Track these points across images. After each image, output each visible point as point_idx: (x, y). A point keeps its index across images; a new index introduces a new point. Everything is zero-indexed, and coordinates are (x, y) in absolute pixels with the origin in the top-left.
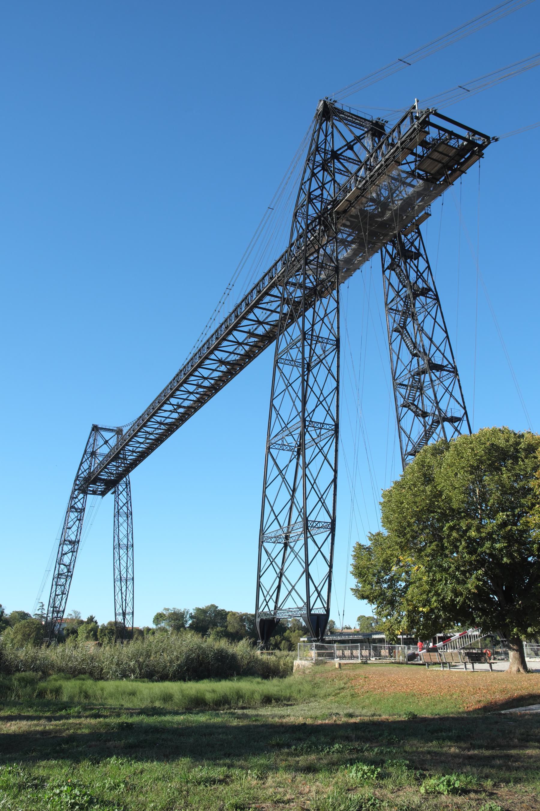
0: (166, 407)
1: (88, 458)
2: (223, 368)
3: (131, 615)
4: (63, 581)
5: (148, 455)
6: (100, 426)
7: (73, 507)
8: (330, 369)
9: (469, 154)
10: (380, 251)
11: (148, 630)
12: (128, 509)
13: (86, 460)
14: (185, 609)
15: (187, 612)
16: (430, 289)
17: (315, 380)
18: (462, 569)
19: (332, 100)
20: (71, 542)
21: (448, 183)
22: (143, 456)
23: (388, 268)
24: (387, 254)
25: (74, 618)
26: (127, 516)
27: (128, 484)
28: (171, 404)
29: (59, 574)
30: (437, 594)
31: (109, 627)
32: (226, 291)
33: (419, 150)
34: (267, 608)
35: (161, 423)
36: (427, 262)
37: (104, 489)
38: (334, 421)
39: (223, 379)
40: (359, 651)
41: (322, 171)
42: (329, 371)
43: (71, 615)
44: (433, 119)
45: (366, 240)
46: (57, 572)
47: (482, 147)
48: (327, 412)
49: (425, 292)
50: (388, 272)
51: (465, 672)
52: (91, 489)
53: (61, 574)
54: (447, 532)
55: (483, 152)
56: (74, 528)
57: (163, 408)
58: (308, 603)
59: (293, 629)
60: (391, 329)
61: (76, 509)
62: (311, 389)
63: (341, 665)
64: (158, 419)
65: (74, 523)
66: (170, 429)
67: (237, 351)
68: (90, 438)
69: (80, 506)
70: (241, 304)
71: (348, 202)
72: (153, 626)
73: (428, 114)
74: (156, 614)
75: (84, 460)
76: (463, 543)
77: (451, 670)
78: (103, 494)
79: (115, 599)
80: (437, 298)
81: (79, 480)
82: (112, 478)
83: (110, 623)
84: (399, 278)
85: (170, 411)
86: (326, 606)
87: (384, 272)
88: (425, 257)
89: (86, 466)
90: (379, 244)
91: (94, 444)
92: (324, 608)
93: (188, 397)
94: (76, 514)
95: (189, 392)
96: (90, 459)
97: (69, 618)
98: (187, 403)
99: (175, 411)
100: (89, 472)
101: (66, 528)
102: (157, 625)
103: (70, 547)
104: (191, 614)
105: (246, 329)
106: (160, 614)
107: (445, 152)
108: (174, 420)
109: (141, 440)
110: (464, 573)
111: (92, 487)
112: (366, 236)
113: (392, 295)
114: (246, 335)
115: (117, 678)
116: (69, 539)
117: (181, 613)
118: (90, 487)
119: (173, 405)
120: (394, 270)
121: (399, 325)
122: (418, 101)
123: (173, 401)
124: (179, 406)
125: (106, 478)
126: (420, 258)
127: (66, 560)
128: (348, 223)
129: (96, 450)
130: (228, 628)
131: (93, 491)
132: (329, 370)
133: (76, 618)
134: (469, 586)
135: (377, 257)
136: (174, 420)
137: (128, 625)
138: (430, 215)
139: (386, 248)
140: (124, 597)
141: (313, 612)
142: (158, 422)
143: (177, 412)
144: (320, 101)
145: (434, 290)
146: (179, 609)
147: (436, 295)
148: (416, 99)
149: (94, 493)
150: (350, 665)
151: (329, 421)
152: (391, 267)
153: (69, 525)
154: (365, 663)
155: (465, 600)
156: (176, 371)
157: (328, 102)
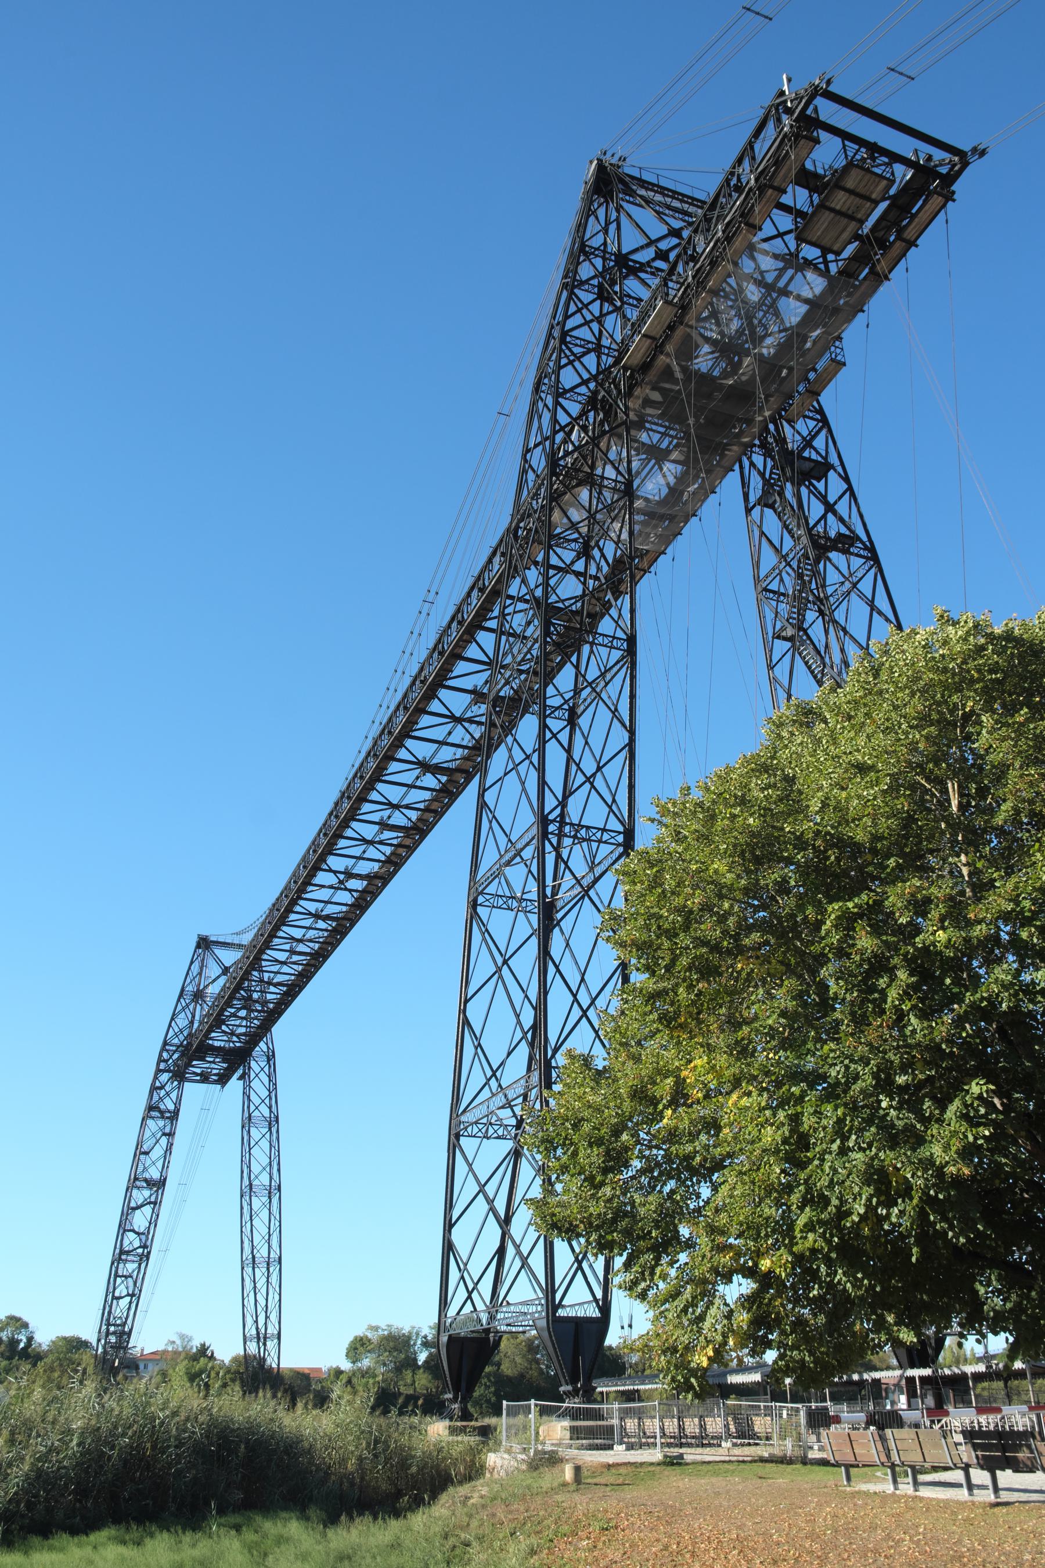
0: (321, 878)
1: (187, 1005)
2: (430, 781)
3: (276, 1341)
4: (131, 1267)
5: (301, 989)
6: (212, 939)
7: (156, 1108)
8: (616, 710)
9: (920, 202)
10: (737, 467)
11: (338, 1372)
12: (271, 1112)
13: (183, 1009)
14: (413, 1328)
15: (417, 1334)
16: (853, 539)
17: (587, 743)
18: (901, 1080)
19: (616, 157)
20: (150, 1183)
21: (879, 278)
22: (292, 991)
23: (759, 502)
24: (754, 473)
25: (180, 1349)
26: (270, 1124)
27: (270, 1057)
28: (330, 870)
29: (122, 1252)
30: (815, 1200)
31: (234, 1367)
32: (422, 607)
33: (799, 197)
34: (468, 1308)
35: (317, 916)
36: (846, 479)
37: (225, 1069)
38: (624, 825)
39: (433, 807)
40: (657, 1421)
41: (598, 302)
42: (613, 713)
43: (174, 1342)
44: (827, 109)
45: (689, 403)
46: (117, 1251)
47: (950, 179)
48: (610, 807)
49: (845, 543)
50: (756, 512)
51: (962, 1504)
52: (198, 1071)
53: (128, 1253)
54: (835, 938)
55: (953, 188)
56: (158, 1152)
57: (317, 880)
58: (550, 1289)
59: (640, 1367)
60: (770, 635)
61: (162, 1112)
62: (578, 765)
63: (585, 1473)
64: (312, 907)
65: (157, 1141)
66: (340, 929)
67: (453, 739)
68: (192, 963)
69: (171, 1107)
70: (449, 626)
71: (649, 341)
72: (346, 1365)
73: (815, 92)
74: (351, 1338)
75: (179, 1008)
76: (902, 975)
77: (925, 1492)
78: (223, 1079)
79: (243, 1305)
80: (873, 557)
81: (167, 1051)
82: (238, 1045)
83: (235, 1360)
84: (780, 519)
85: (331, 887)
86: (599, 1294)
87: (748, 511)
88: (840, 469)
89: (182, 1021)
90: (735, 448)
91: (200, 974)
92: (596, 1300)
93: (364, 852)
94: (161, 1123)
95: (364, 840)
96: (191, 1007)
97: (170, 1349)
98: (364, 868)
99: (340, 886)
100: (190, 1035)
101: (141, 1152)
102: (354, 1362)
103: (146, 1193)
104: (425, 1337)
105: (467, 683)
106: (361, 1339)
107: (860, 190)
108: (344, 909)
109: (282, 956)
110: (909, 1096)
111: (198, 1067)
112: (688, 395)
113: (769, 559)
114: (468, 698)
115: (578, 1449)
116: (147, 1175)
117: (404, 1335)
118: (193, 1066)
119: (335, 872)
120: (772, 506)
121: (788, 620)
122: (789, 80)
123: (333, 862)
124: (349, 875)
125: (222, 1044)
126: (831, 474)
127: (140, 1220)
128: (656, 396)
129: (206, 987)
130: (502, 1367)
131: (201, 1075)
132: (615, 712)
133: (184, 1348)
134: (936, 1150)
135: (732, 481)
136: (344, 909)
137: (271, 1362)
138: (844, 364)
139: (749, 458)
140: (262, 1301)
141: (561, 1313)
142: (310, 914)
143: (346, 889)
144: (591, 162)
145: (865, 538)
146: (400, 1326)
147: (872, 549)
148: (784, 77)
149: (205, 1078)
150: (623, 1470)
151: (614, 825)
152: (765, 502)
153: (145, 1148)
154: (673, 1462)
155: (922, 1215)
156: (335, 796)
157: (608, 159)
